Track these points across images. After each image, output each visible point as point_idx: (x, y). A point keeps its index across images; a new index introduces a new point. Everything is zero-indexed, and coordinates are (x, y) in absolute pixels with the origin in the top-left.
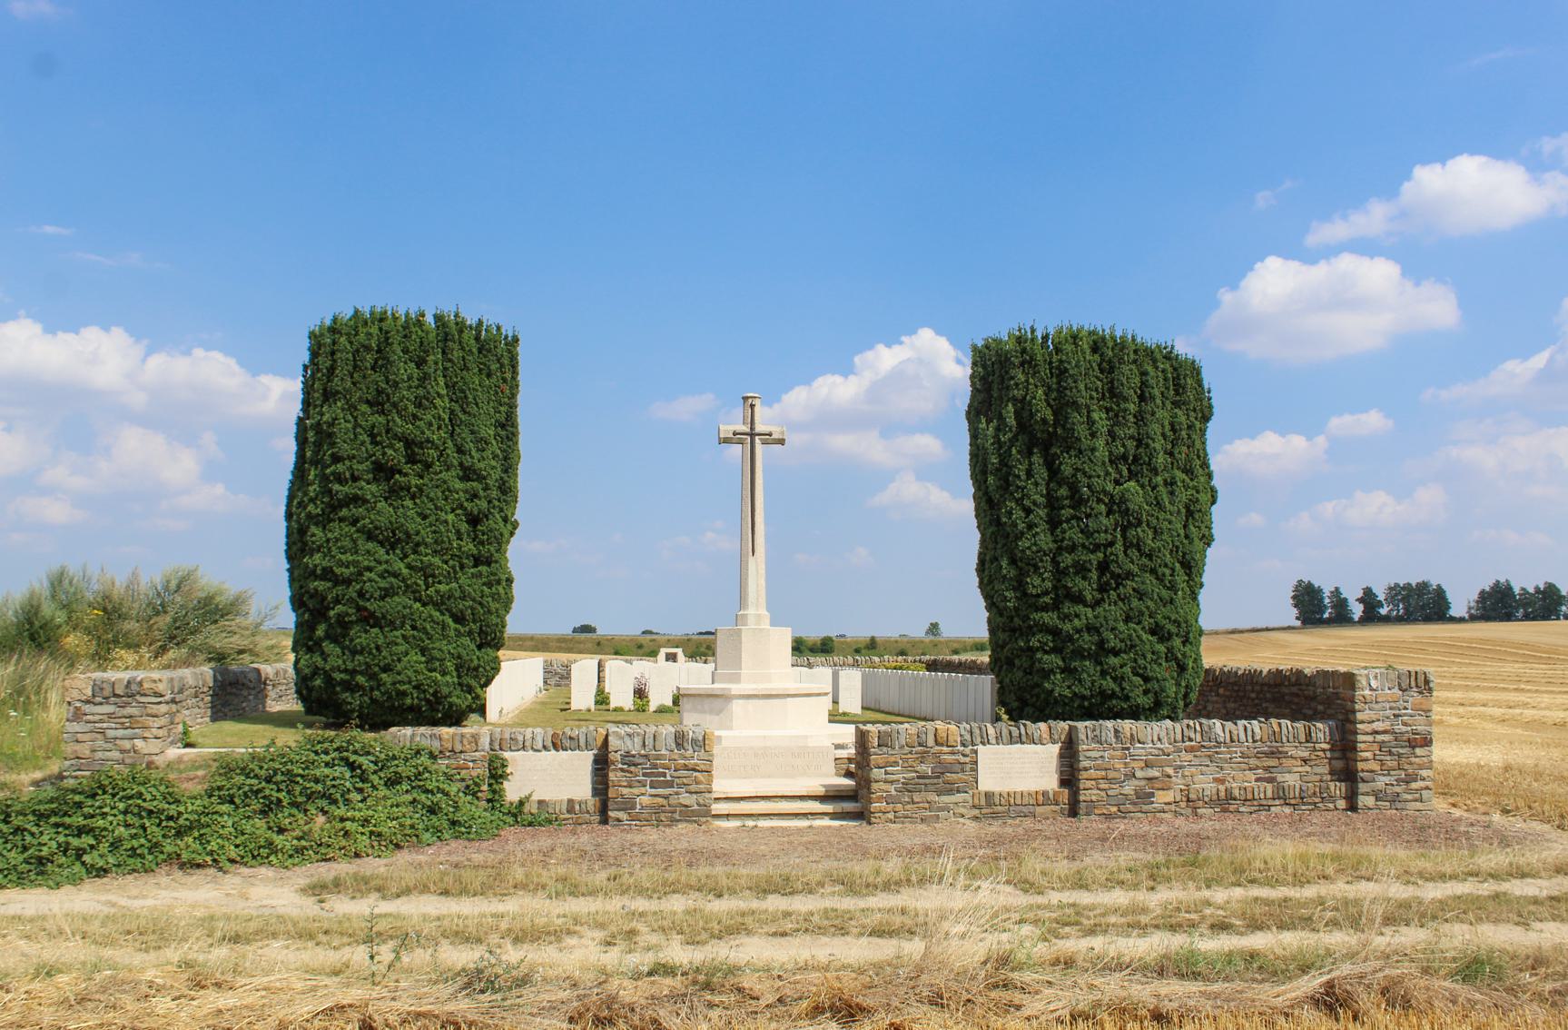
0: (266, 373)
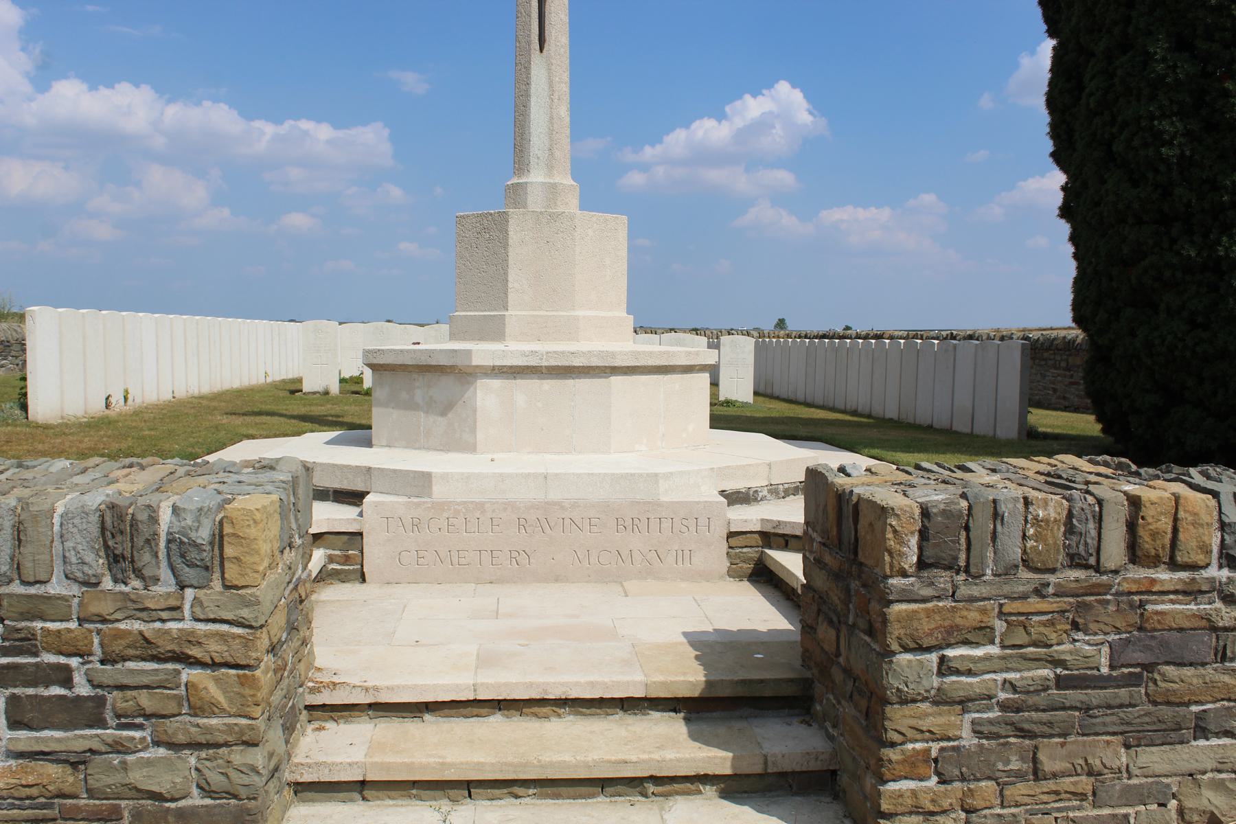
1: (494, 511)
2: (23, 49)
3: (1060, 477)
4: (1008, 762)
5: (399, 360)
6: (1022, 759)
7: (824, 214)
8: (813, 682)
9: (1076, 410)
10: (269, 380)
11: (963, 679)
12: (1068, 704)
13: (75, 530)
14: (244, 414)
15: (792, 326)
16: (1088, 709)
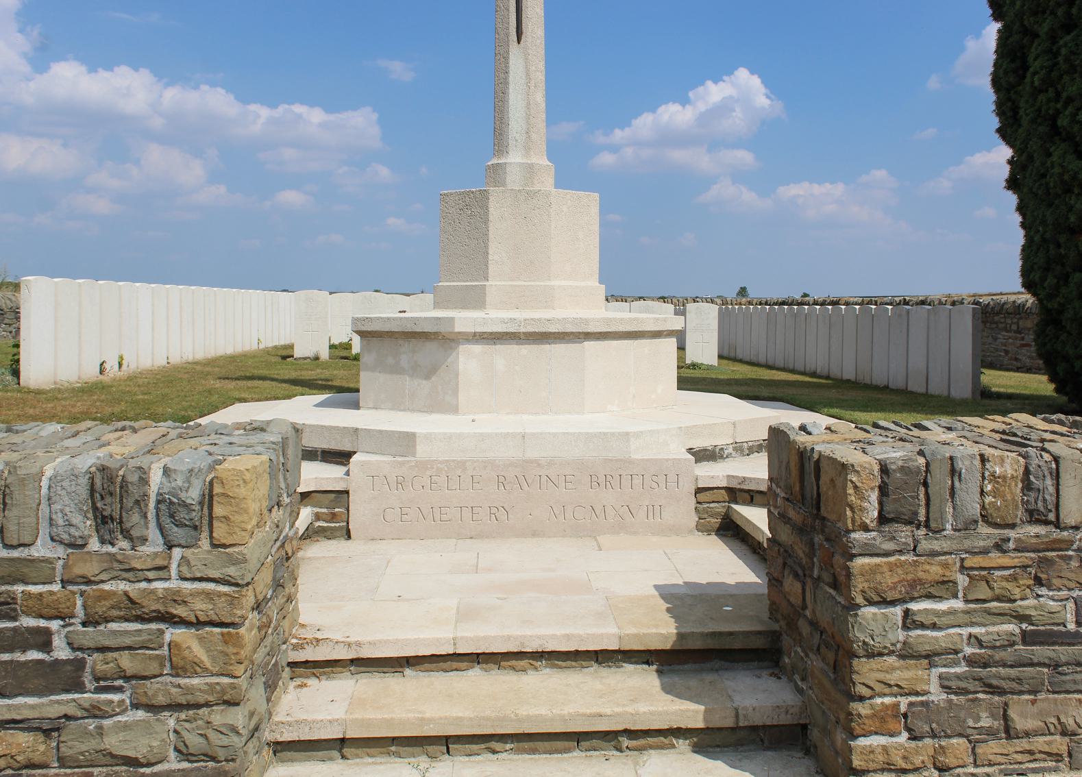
0: (255, 102)
1: (474, 469)
2: (21, 31)
3: (1015, 435)
4: (978, 719)
5: (387, 327)
6: (993, 716)
7: (781, 189)
8: (781, 634)
9: (1029, 370)
10: (262, 346)
11: (928, 633)
12: (1036, 661)
13: (64, 493)
14: (237, 379)
15: (753, 294)
16: (1057, 666)
